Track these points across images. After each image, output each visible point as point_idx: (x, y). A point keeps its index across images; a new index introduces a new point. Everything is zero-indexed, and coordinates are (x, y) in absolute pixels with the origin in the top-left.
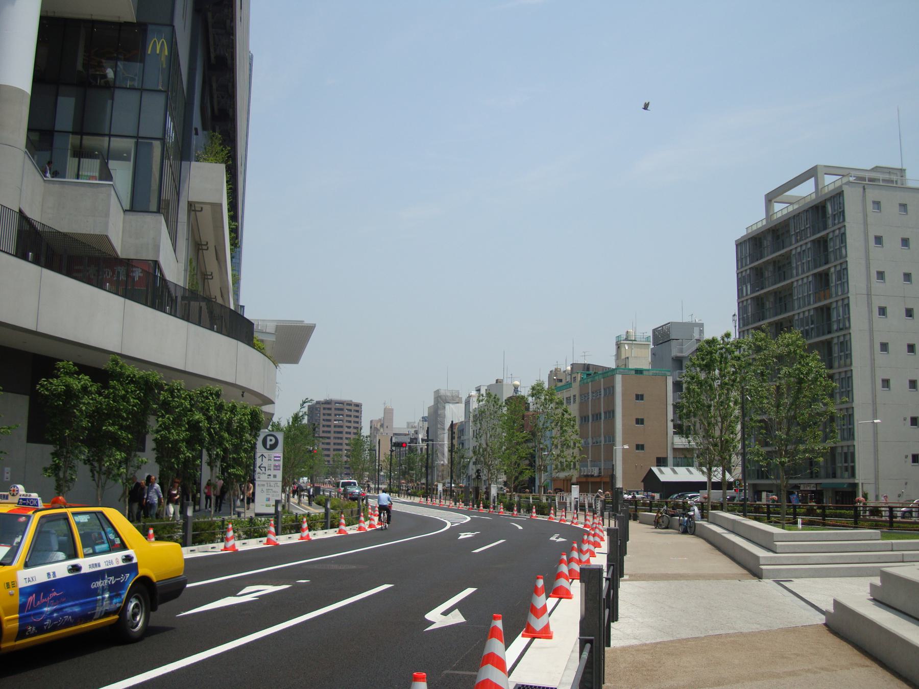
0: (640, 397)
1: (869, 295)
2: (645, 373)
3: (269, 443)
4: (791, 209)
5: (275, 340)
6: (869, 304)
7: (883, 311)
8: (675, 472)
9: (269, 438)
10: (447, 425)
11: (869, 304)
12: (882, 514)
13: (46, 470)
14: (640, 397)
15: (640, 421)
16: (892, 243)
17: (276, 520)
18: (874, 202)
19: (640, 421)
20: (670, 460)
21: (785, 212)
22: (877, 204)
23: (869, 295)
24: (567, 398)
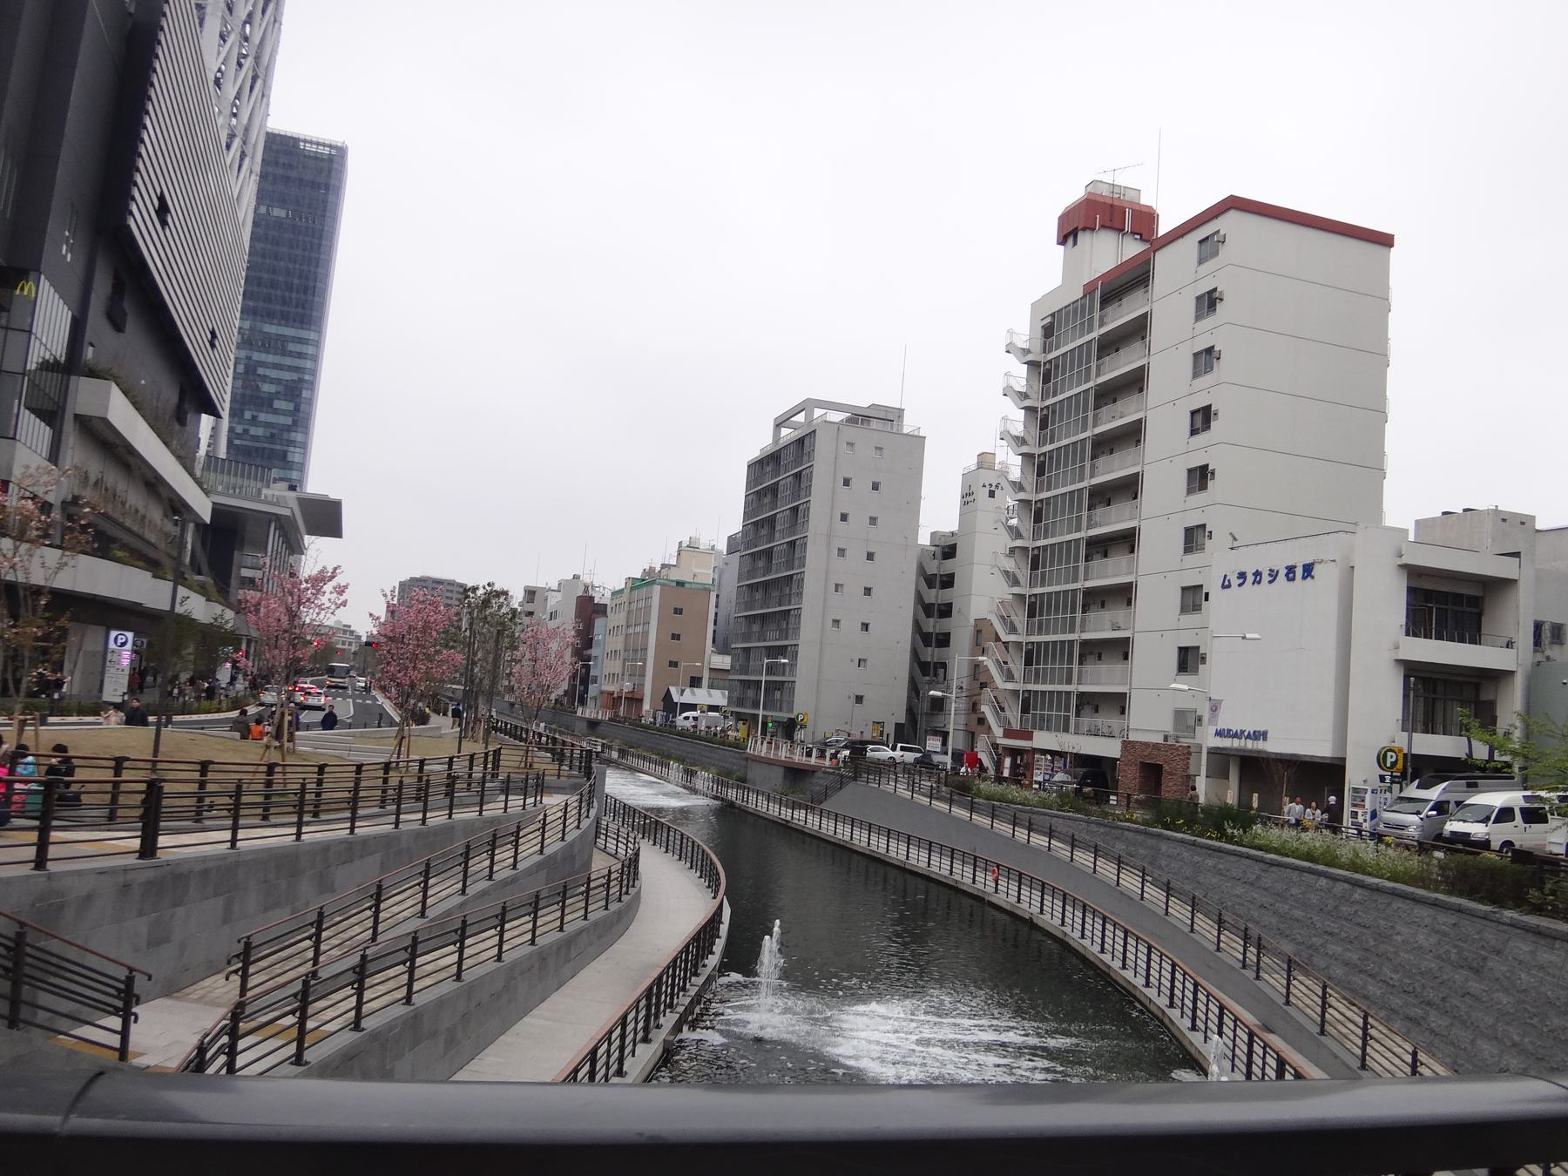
0: (678, 611)
1: (829, 536)
2: (687, 585)
3: (119, 641)
4: (796, 433)
5: (297, 733)
6: (829, 544)
7: (842, 552)
8: (710, 695)
9: (1389, 754)
10: (972, 622)
11: (829, 544)
12: (1088, 785)
13: (1313, 577)
14: (678, 611)
15: (676, 637)
16: (861, 485)
17: (268, 380)
18: (848, 443)
19: (676, 637)
20: (705, 682)
21: (792, 435)
22: (851, 444)
23: (829, 536)
24: (1304, 566)
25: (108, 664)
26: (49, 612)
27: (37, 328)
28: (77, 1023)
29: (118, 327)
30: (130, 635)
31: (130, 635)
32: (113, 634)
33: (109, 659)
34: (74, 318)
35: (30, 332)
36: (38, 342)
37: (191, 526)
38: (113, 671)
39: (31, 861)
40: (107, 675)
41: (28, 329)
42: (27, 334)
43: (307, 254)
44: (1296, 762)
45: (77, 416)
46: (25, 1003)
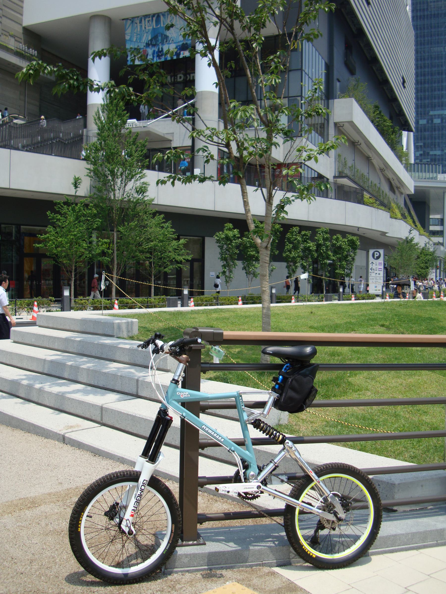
3: (376, 256)
25: (370, 271)
26: (339, 290)
27: (306, 68)
28: (12, 396)
29: (352, 72)
30: (382, 251)
31: (382, 251)
32: (371, 252)
33: (370, 268)
34: (326, 64)
35: (301, 70)
36: (307, 77)
37: (413, 125)
38: (373, 275)
39: (244, 193)
40: (370, 278)
41: (300, 68)
42: (299, 72)
43: (440, 133)
44: (352, 563)
45: (336, 124)
46: (175, 447)
